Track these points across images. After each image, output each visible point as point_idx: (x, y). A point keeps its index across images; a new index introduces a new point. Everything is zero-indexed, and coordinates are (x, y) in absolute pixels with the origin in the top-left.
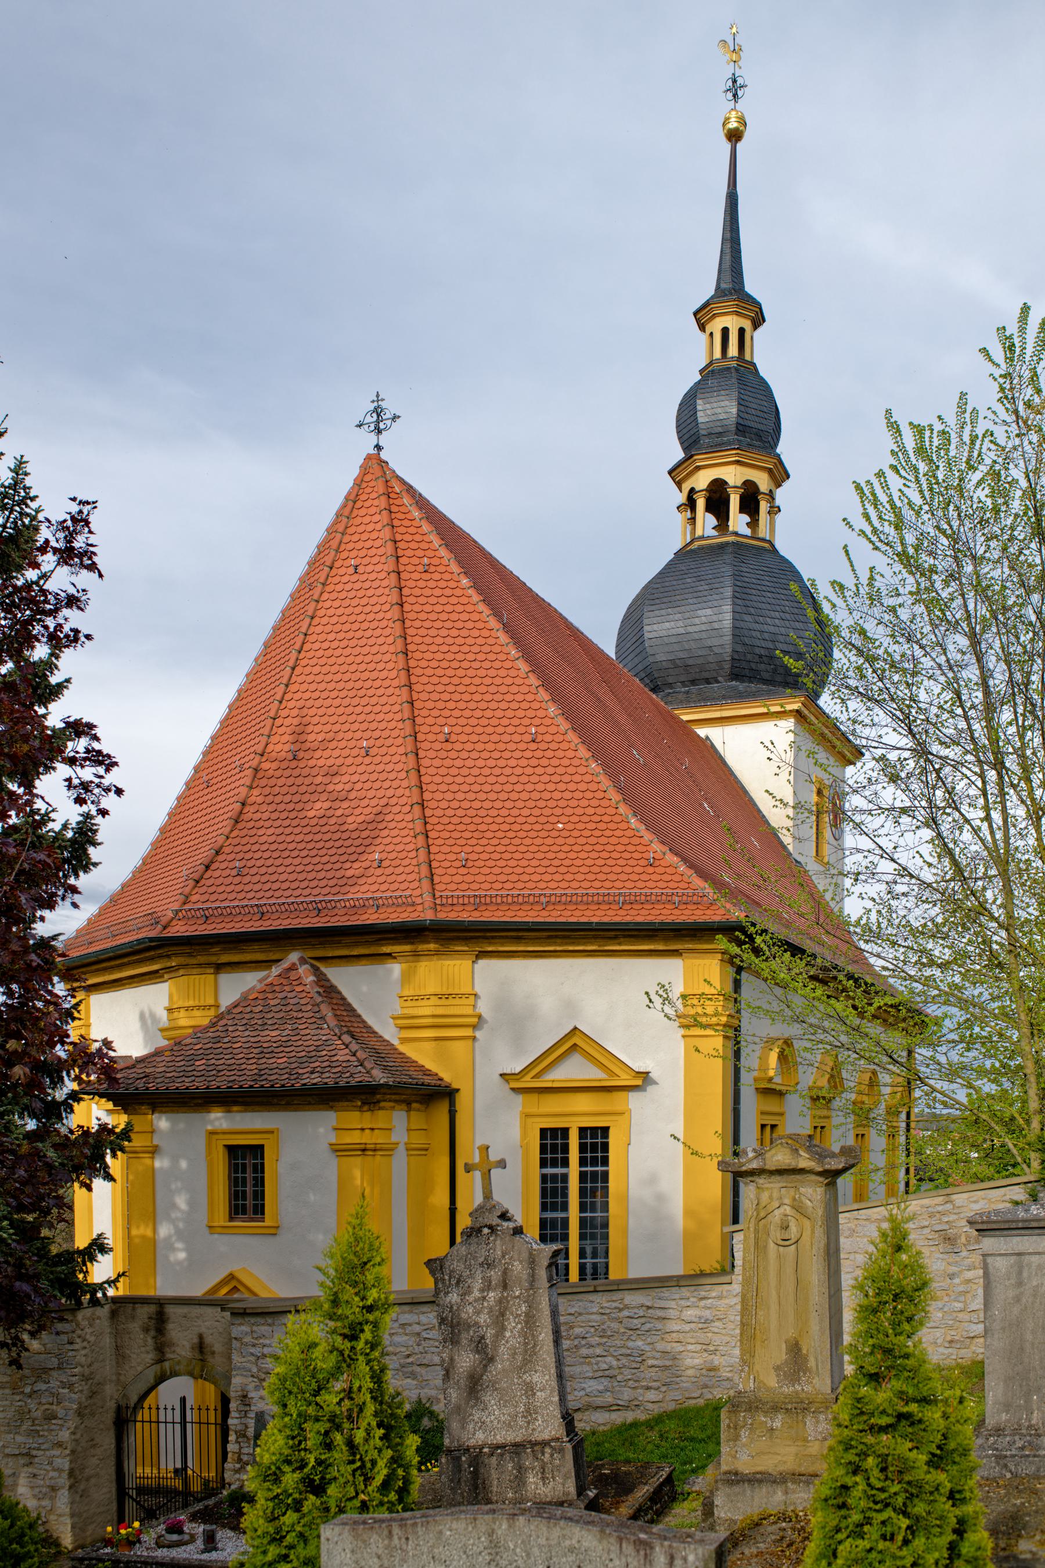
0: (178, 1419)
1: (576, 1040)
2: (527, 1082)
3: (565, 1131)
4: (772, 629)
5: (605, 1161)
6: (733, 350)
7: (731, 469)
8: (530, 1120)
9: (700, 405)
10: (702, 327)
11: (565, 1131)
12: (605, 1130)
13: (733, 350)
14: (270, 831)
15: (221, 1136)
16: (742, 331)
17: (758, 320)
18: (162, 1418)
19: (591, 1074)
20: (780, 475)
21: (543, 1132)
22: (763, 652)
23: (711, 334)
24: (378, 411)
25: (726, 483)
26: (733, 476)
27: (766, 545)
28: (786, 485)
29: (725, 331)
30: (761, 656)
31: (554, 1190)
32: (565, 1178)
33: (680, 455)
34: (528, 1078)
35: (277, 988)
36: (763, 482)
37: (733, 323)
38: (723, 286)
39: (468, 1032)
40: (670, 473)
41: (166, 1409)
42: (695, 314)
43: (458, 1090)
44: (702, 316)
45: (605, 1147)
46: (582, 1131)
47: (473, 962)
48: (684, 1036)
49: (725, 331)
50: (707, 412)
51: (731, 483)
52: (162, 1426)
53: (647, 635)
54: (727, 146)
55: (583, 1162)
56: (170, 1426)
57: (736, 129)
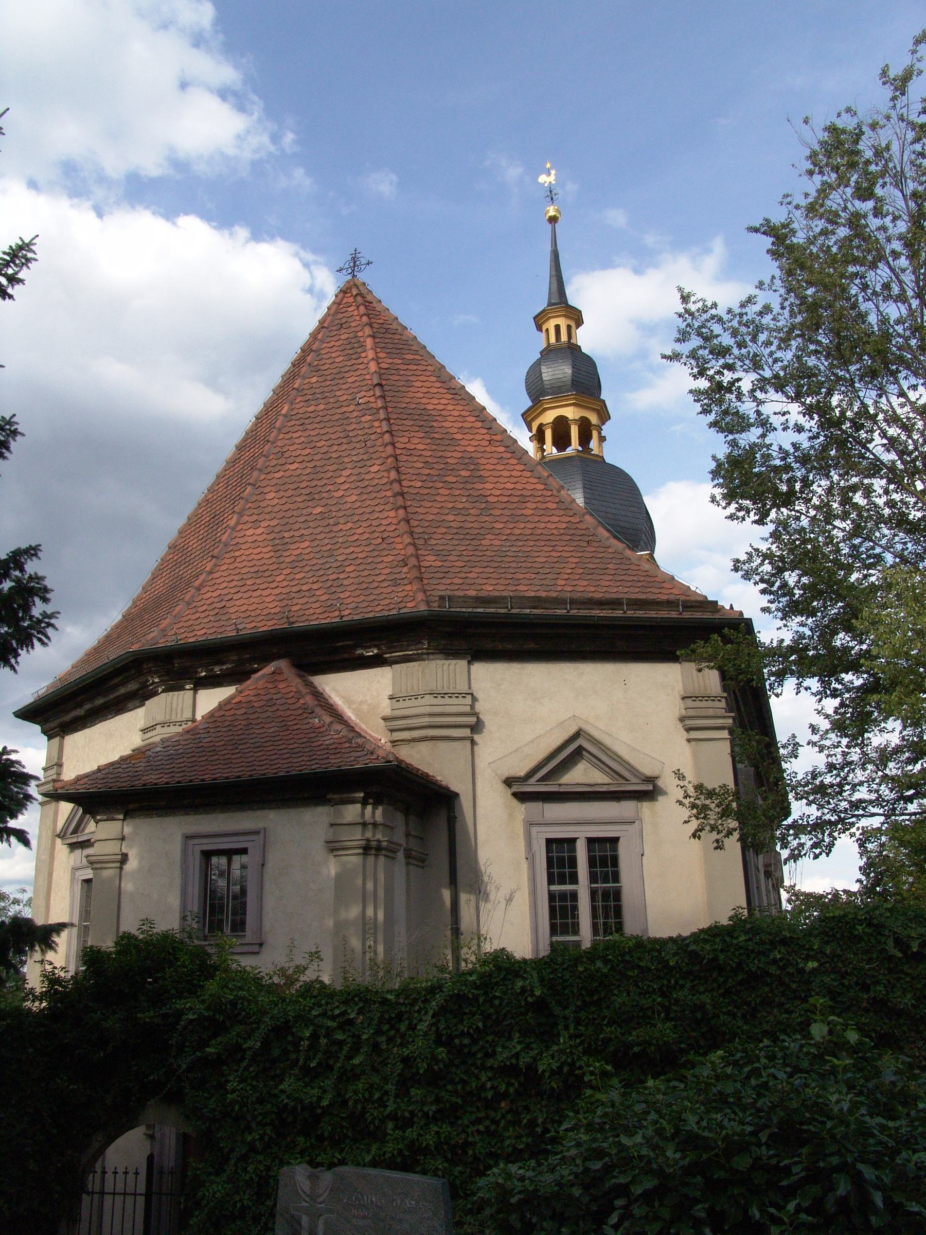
0: (142, 1188)
1: (580, 742)
2: (531, 787)
3: (572, 841)
4: (614, 511)
5: (616, 877)
6: (564, 338)
7: (571, 409)
8: (534, 830)
9: (544, 369)
10: (539, 328)
11: (572, 841)
12: (615, 841)
13: (564, 338)
15: (196, 841)
16: (569, 327)
17: (579, 322)
18: (109, 1187)
20: (604, 416)
21: (549, 842)
23: (547, 330)
24: (354, 260)
26: (570, 413)
27: (600, 460)
28: (608, 423)
29: (557, 328)
31: (564, 909)
32: (574, 896)
33: (531, 404)
34: (533, 780)
36: (594, 419)
37: (563, 322)
38: (553, 301)
39: (466, 732)
40: (523, 415)
41: (115, 1173)
42: (534, 318)
43: (716, 922)
44: (539, 321)
45: (615, 861)
46: (591, 841)
47: (469, 662)
48: (689, 740)
49: (557, 328)
50: (548, 374)
52: (108, 1199)
54: (549, 227)
55: (593, 878)
56: (129, 1200)
57: (555, 216)
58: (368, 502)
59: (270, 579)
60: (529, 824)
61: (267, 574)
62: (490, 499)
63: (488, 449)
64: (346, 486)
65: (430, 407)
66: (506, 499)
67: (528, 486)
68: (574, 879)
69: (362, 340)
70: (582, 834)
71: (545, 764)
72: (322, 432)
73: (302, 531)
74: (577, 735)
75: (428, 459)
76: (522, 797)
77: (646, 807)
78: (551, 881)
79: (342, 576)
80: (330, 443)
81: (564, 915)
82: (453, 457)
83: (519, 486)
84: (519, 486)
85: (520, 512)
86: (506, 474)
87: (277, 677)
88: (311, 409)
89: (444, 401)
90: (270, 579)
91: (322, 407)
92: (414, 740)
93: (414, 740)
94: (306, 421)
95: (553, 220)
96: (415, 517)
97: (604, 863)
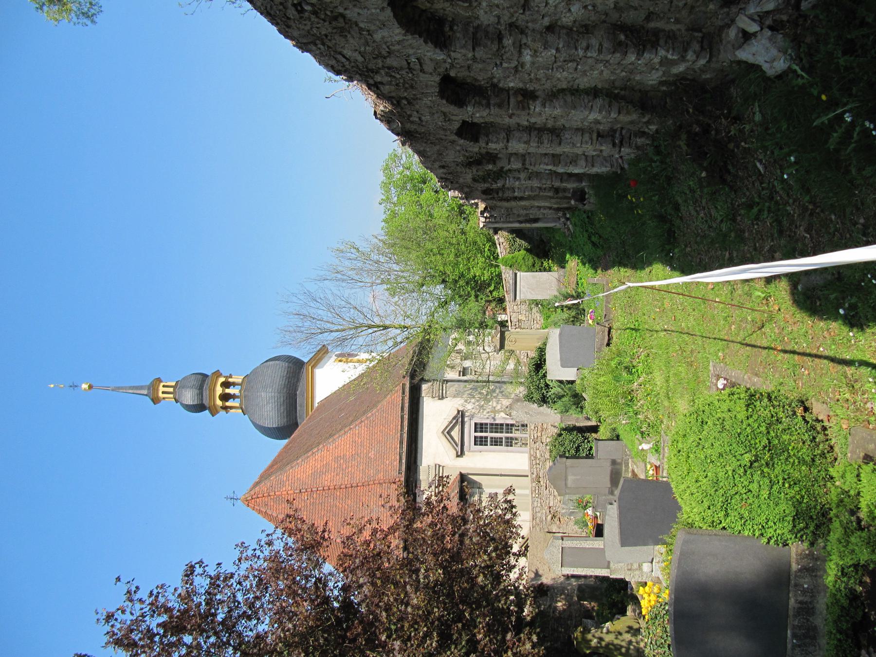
2: (459, 449)
11: (475, 437)
13: (171, 390)
16: (164, 386)
21: (475, 444)
29: (163, 393)
32: (492, 438)
36: (222, 380)
39: (441, 468)
46: (475, 431)
49: (163, 393)
55: (486, 432)
60: (469, 451)
62: (354, 453)
65: (310, 472)
67: (348, 439)
68: (486, 438)
70: (473, 434)
78: (487, 445)
81: (497, 442)
83: (348, 442)
84: (348, 442)
85: (359, 444)
86: (342, 446)
95: (91, 387)
97: (497, 442)
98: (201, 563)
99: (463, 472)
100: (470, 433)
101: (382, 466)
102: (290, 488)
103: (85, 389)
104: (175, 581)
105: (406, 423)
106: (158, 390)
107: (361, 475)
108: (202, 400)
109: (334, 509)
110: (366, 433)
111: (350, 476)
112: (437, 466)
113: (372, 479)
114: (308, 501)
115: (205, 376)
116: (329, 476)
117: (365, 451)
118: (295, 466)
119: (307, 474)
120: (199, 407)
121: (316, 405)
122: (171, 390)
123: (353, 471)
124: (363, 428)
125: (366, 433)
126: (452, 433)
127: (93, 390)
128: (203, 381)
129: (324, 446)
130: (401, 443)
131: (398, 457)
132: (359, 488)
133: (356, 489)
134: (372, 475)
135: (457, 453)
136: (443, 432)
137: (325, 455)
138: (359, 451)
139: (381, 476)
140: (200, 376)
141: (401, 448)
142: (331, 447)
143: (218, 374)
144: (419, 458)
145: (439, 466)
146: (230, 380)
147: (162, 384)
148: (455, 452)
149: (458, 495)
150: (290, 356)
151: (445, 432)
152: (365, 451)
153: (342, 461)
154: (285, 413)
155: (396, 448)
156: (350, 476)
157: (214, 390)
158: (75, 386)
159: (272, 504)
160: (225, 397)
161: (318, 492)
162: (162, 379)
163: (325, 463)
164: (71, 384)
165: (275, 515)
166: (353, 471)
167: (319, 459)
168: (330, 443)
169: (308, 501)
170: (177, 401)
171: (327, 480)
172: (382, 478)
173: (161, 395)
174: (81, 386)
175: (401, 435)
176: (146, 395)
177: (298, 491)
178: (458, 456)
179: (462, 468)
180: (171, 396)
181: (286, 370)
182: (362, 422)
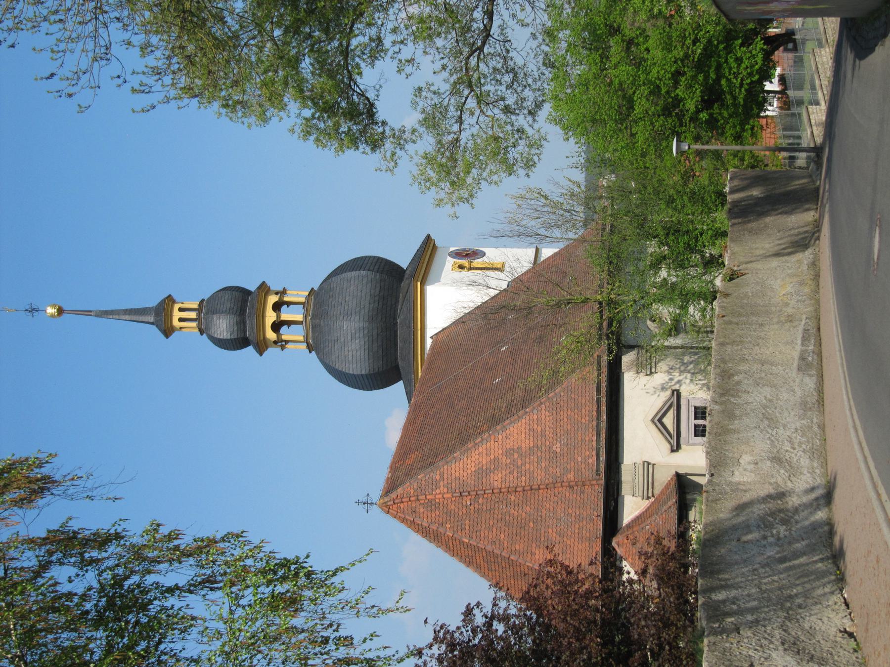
2: (674, 442)
8: (691, 441)
11: (696, 426)
12: (696, 408)
13: (193, 315)
14: (591, 528)
16: (181, 310)
19: (671, 415)
21: (696, 435)
22: (381, 303)
25: (274, 322)
30: (383, 304)
35: (460, 523)
36: (273, 299)
39: (651, 466)
46: (696, 418)
51: (275, 319)
53: (359, 373)
58: (532, 501)
59: (568, 547)
61: (565, 548)
62: (532, 445)
63: (500, 443)
64: (520, 511)
65: (473, 469)
66: (531, 438)
69: (426, 501)
71: (431, 255)
72: (484, 522)
73: (543, 531)
74: (653, 421)
75: (508, 472)
76: (679, 447)
77: (684, 394)
79: (574, 514)
80: (492, 518)
82: (505, 460)
87: (621, 543)
88: (467, 527)
89: (469, 462)
90: (568, 547)
91: (467, 522)
92: (653, 488)
93: (653, 488)
94: (475, 529)
95: (61, 311)
96: (543, 481)
98: (478, 604)
99: (680, 472)
100: (688, 422)
101: (572, 464)
102: (446, 490)
103: (52, 316)
104: (454, 621)
105: (604, 409)
106: (171, 316)
107: (543, 474)
108: (244, 331)
109: (507, 518)
110: (548, 419)
111: (528, 476)
112: (646, 464)
113: (558, 480)
114: (472, 507)
115: (245, 293)
116: (500, 475)
117: (547, 443)
118: (451, 461)
119: (469, 472)
120: (239, 342)
121: (429, 342)
122: (193, 315)
123: (532, 469)
124: (543, 411)
125: (548, 419)
126: (665, 420)
127: (65, 316)
128: (244, 302)
129: (490, 435)
130: (598, 435)
131: (594, 453)
132: (541, 491)
133: (537, 492)
134: (558, 474)
135: (672, 447)
136: (653, 421)
137: (492, 447)
138: (540, 443)
139: (571, 476)
140: (237, 294)
141: (598, 441)
142: (500, 437)
143: (264, 289)
144: (620, 451)
145: (649, 464)
146: (286, 299)
147: (177, 307)
148: (668, 446)
149: (677, 505)
150: (379, 258)
151: (656, 420)
152: (547, 443)
153: (516, 456)
154: (380, 352)
155: (591, 441)
156: (528, 476)
157: (263, 316)
158: (32, 310)
159: (422, 510)
160: (277, 326)
161: (486, 496)
162: (175, 297)
163: (492, 457)
164: (28, 307)
165: (425, 524)
166: (532, 469)
167: (485, 452)
168: (498, 431)
169: (472, 507)
170: (202, 332)
171: (497, 480)
172: (572, 479)
173: (176, 323)
174: (45, 311)
175: (598, 425)
176: (152, 323)
177: (458, 495)
178: (672, 451)
179: (679, 466)
180: (194, 324)
181: (378, 285)
182: (541, 403)
